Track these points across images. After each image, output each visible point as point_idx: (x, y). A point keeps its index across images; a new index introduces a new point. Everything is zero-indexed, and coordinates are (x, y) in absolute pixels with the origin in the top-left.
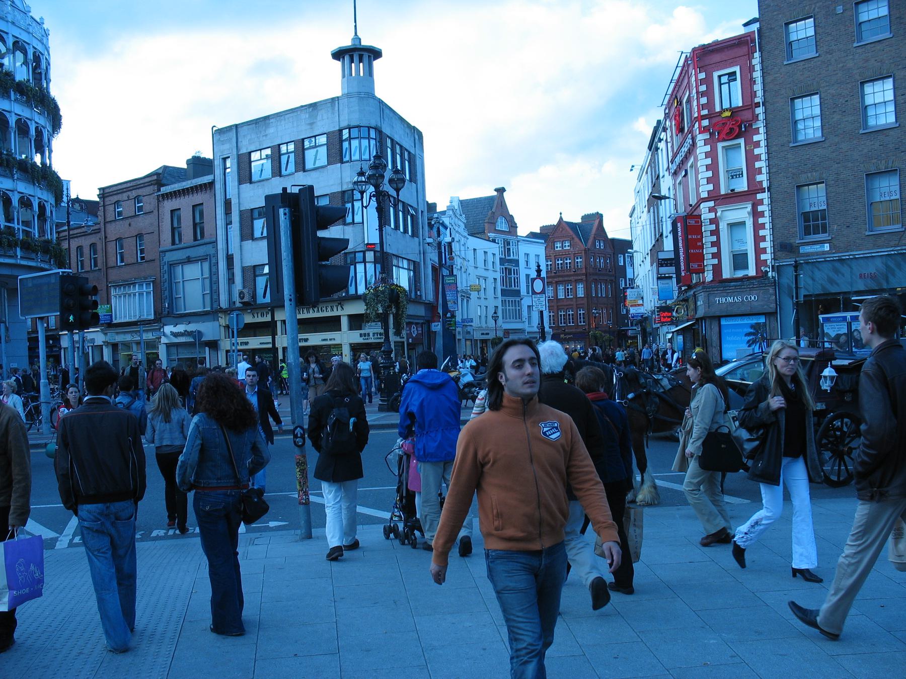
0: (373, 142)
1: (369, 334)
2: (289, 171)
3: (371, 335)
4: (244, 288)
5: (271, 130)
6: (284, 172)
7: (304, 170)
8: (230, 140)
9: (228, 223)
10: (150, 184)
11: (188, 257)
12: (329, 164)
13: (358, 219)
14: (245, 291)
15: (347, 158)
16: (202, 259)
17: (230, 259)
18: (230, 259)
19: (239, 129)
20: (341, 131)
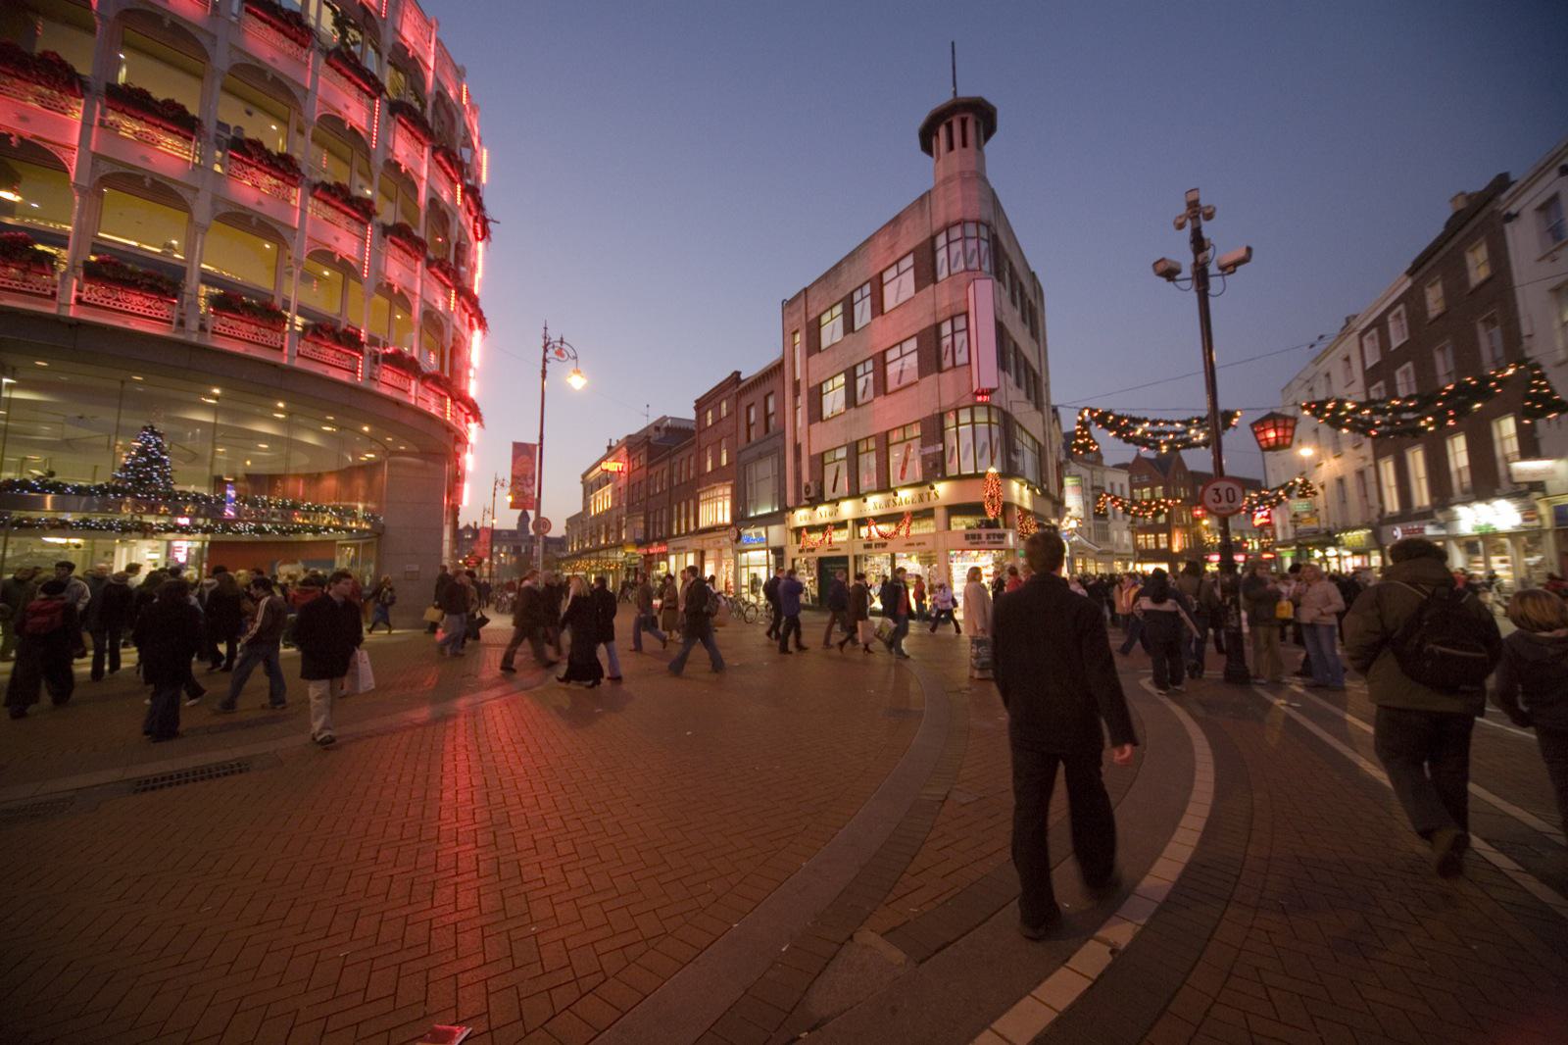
0: (984, 245)
1: (980, 536)
2: (866, 400)
3: (984, 538)
4: (811, 480)
5: (844, 277)
6: (860, 400)
7: (886, 394)
8: (799, 309)
9: (796, 408)
10: (730, 385)
11: (760, 453)
12: (920, 377)
13: (961, 358)
14: (812, 484)
15: (947, 363)
16: (768, 454)
17: (797, 449)
18: (797, 449)
19: (809, 293)
20: (937, 327)
